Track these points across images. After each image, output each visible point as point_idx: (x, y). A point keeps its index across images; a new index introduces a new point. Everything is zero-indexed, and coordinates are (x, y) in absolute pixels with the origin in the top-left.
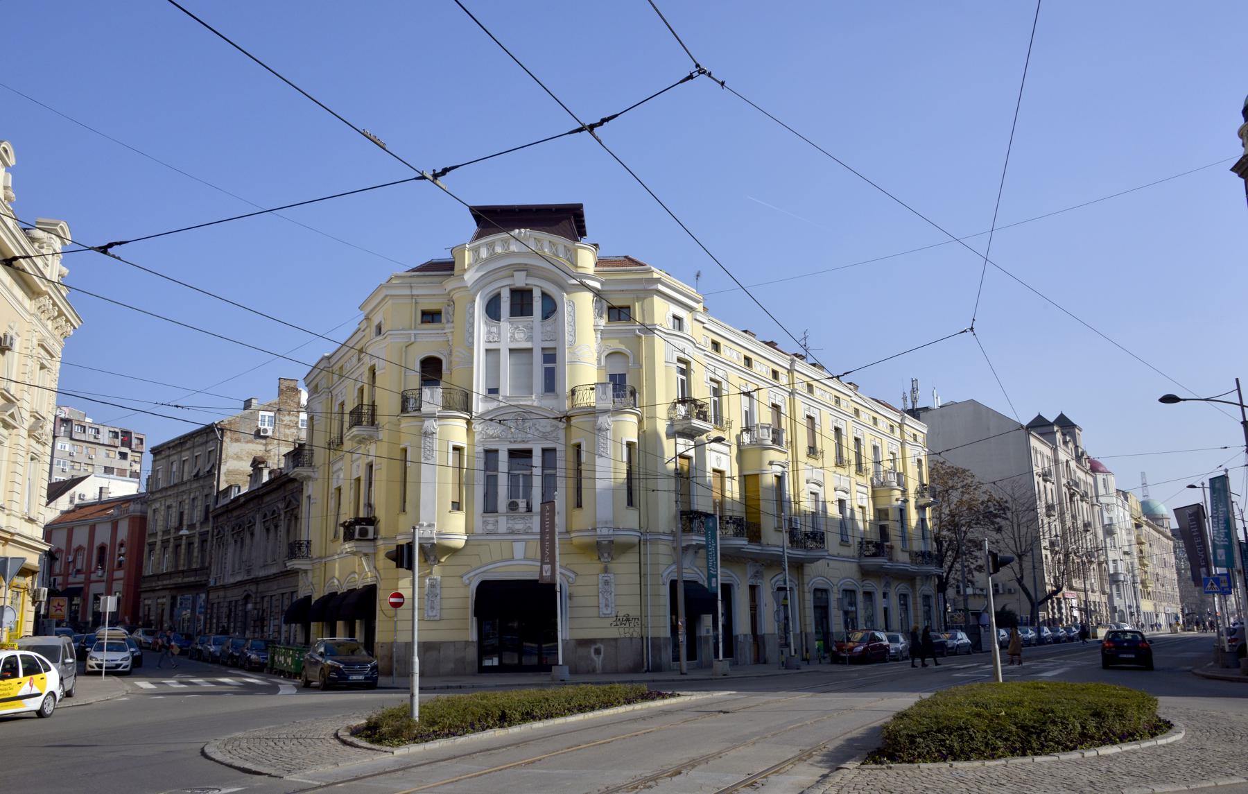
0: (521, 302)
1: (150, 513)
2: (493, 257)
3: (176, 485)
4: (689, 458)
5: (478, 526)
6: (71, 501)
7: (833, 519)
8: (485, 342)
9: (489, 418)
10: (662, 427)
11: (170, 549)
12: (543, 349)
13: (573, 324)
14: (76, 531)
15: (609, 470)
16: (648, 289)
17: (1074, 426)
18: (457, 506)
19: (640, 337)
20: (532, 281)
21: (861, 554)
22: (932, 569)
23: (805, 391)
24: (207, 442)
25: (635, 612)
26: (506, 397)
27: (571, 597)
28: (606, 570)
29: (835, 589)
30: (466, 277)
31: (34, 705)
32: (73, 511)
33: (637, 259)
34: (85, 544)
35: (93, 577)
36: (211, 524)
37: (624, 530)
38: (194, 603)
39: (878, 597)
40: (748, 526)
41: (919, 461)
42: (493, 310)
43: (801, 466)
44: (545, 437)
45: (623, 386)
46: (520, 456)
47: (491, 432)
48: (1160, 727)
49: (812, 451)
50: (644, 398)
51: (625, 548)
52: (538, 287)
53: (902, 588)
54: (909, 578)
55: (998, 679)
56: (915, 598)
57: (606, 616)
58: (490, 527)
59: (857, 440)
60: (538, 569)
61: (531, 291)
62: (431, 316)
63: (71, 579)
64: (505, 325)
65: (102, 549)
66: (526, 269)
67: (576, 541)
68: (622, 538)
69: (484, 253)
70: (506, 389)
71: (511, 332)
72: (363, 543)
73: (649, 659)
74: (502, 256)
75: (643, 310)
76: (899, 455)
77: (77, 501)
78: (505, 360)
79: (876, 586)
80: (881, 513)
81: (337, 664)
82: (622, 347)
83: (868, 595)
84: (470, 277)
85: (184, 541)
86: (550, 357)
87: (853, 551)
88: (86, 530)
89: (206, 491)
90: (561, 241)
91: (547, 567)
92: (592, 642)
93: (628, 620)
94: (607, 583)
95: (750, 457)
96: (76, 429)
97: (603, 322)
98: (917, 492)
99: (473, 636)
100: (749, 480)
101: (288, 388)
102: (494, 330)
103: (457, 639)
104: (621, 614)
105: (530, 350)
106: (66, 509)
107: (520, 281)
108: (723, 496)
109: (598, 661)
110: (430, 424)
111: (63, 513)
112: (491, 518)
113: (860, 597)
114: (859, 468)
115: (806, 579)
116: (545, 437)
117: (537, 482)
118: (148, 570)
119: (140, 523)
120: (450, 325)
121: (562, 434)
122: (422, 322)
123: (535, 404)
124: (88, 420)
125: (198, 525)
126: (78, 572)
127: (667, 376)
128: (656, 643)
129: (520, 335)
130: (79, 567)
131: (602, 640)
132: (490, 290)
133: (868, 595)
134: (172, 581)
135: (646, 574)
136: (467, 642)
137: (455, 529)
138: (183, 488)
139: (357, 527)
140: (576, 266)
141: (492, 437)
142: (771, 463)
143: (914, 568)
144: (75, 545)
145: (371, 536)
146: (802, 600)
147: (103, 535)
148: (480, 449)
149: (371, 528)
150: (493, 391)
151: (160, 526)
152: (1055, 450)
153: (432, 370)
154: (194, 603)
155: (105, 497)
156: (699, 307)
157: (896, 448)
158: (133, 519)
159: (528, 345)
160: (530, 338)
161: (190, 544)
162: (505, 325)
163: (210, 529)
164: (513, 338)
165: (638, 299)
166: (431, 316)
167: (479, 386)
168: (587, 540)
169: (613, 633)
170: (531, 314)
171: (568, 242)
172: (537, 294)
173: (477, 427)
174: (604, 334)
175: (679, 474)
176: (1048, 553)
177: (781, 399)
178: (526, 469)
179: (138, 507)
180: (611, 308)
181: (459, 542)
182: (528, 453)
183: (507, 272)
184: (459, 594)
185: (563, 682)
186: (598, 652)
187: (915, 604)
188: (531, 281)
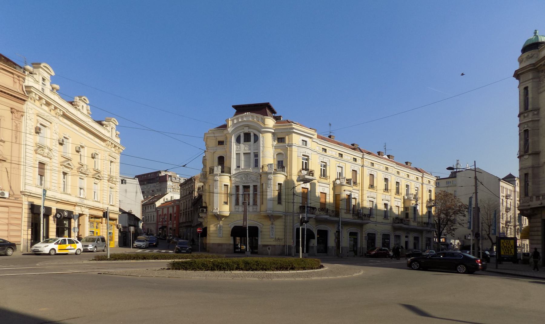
0: (247, 138)
2: (238, 122)
4: (307, 189)
5: (233, 209)
7: (380, 210)
8: (236, 151)
9: (237, 175)
10: (295, 178)
13: (263, 144)
15: (272, 192)
16: (290, 132)
18: (226, 203)
23: (370, 165)
28: (272, 224)
29: (379, 234)
30: (229, 130)
31: (74, 251)
34: (166, 213)
42: (238, 140)
44: (254, 181)
45: (281, 165)
46: (246, 188)
47: (237, 180)
48: (322, 267)
49: (372, 186)
50: (287, 169)
51: (278, 217)
52: (252, 132)
53: (416, 235)
56: (422, 238)
61: (250, 134)
62: (221, 143)
64: (242, 145)
66: (248, 126)
70: (242, 166)
71: (244, 148)
73: (287, 251)
78: (242, 157)
80: (406, 208)
82: (282, 152)
84: (230, 130)
86: (256, 155)
88: (161, 210)
90: (260, 116)
94: (272, 228)
95: (337, 189)
96: (173, 179)
97: (275, 143)
100: (336, 197)
104: (277, 237)
107: (246, 130)
109: (269, 251)
110: (218, 178)
112: (237, 207)
116: (254, 181)
117: (251, 196)
118: (181, 221)
121: (259, 181)
124: (178, 176)
127: (298, 160)
131: (271, 245)
132: (237, 133)
137: (226, 210)
142: (344, 191)
143: (421, 228)
145: (205, 212)
146: (362, 236)
147: (171, 211)
148: (234, 185)
149: (205, 209)
150: (239, 167)
152: (515, 187)
153: (221, 160)
155: (173, 199)
156: (315, 137)
157: (419, 186)
158: (177, 206)
159: (249, 152)
160: (250, 149)
165: (287, 135)
166: (221, 143)
169: (274, 243)
170: (250, 141)
171: (262, 116)
172: (252, 134)
173: (233, 179)
174: (276, 147)
175: (303, 193)
177: (358, 168)
178: (247, 192)
181: (227, 214)
184: (228, 230)
185: (248, 256)
186: (269, 249)
187: (422, 240)
188: (250, 130)
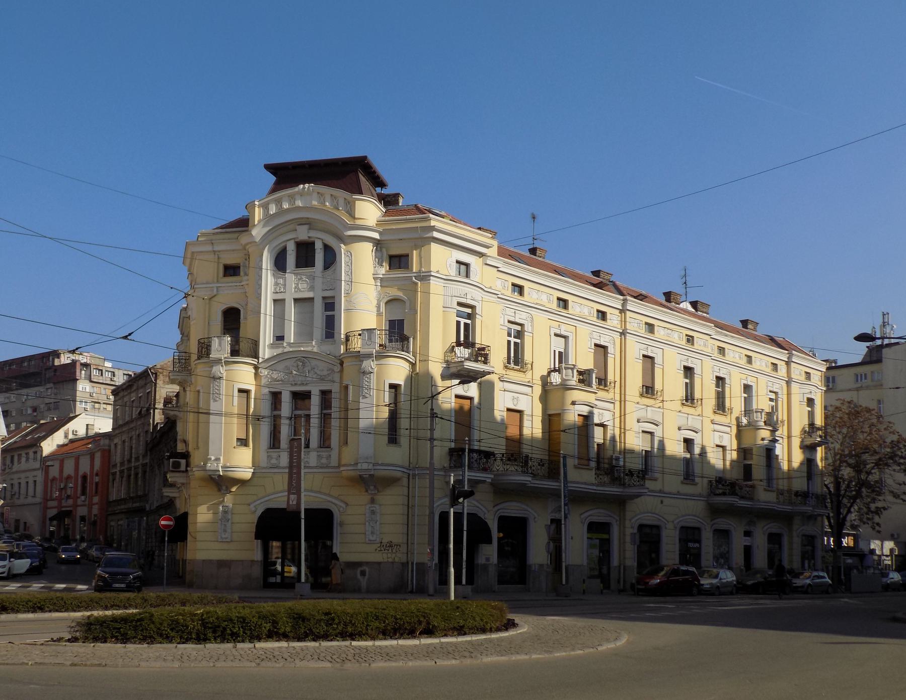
0: (305, 254)
1: (113, 447)
2: (281, 212)
3: (127, 423)
6: (66, 436)
7: (673, 458)
10: (436, 369)
11: (124, 479)
12: (324, 298)
13: (350, 273)
14: (66, 462)
15: (374, 410)
16: (424, 238)
18: (243, 442)
19: (417, 284)
20: (313, 234)
24: (146, 384)
25: (398, 539)
26: (289, 344)
27: (341, 524)
28: (373, 501)
29: (670, 526)
32: (66, 445)
35: (79, 502)
36: (149, 457)
37: (382, 465)
38: (140, 524)
40: (552, 465)
41: (810, 402)
42: (280, 264)
43: (630, 407)
44: (322, 379)
45: (399, 333)
46: (301, 397)
49: (649, 390)
51: (390, 482)
52: (320, 240)
53: (774, 527)
55: (447, 594)
57: (371, 542)
58: (274, 461)
60: (286, 499)
61: (313, 244)
62: (231, 270)
63: (64, 504)
64: (291, 278)
65: (84, 477)
66: (309, 223)
67: (344, 473)
68: (382, 472)
69: (273, 209)
70: (291, 336)
71: (295, 284)
72: (177, 474)
74: (288, 211)
75: (420, 257)
76: (783, 397)
77: (71, 436)
78: (291, 311)
80: (744, 452)
81: (104, 574)
82: (400, 294)
83: (723, 534)
84: (257, 232)
85: (140, 470)
86: (330, 305)
88: (57, 464)
89: (146, 429)
90: (341, 194)
91: (293, 497)
92: (359, 564)
93: (391, 546)
94: (373, 512)
95: (553, 397)
96: (95, 373)
97: (383, 270)
98: (804, 431)
100: (551, 420)
102: (281, 281)
104: (385, 541)
105: (311, 300)
106: (61, 443)
107: (303, 234)
108: (521, 434)
109: (364, 582)
110: (221, 370)
111: (59, 446)
112: (274, 453)
114: (721, 406)
115: (629, 515)
116: (322, 379)
117: (315, 422)
118: (113, 497)
119: (107, 454)
120: (246, 278)
121: (337, 377)
122: (225, 275)
123: (315, 350)
124: (108, 364)
125: (141, 457)
126: (68, 497)
128: (422, 568)
129: (303, 286)
130: (69, 493)
131: (367, 563)
132: (278, 243)
133: (723, 534)
134: (126, 506)
135: (413, 506)
136: (252, 561)
137: (242, 462)
138: (132, 425)
140: (354, 218)
141: (276, 380)
142: (573, 403)
143: (788, 508)
144: (65, 475)
145: (183, 468)
147: (85, 467)
149: (183, 462)
150: (280, 338)
151: (118, 459)
153: (232, 320)
154: (140, 524)
155: (91, 433)
156: (493, 252)
157: (780, 386)
160: (312, 288)
161: (136, 474)
162: (291, 278)
163: (148, 461)
165: (416, 247)
166: (231, 270)
167: (266, 336)
168: (352, 473)
172: (319, 246)
173: (264, 372)
174: (384, 282)
175: (459, 411)
178: (303, 411)
179: (107, 442)
180: (391, 257)
183: (292, 227)
184: (246, 519)
185: (302, 597)
186: (363, 573)
188: (313, 234)
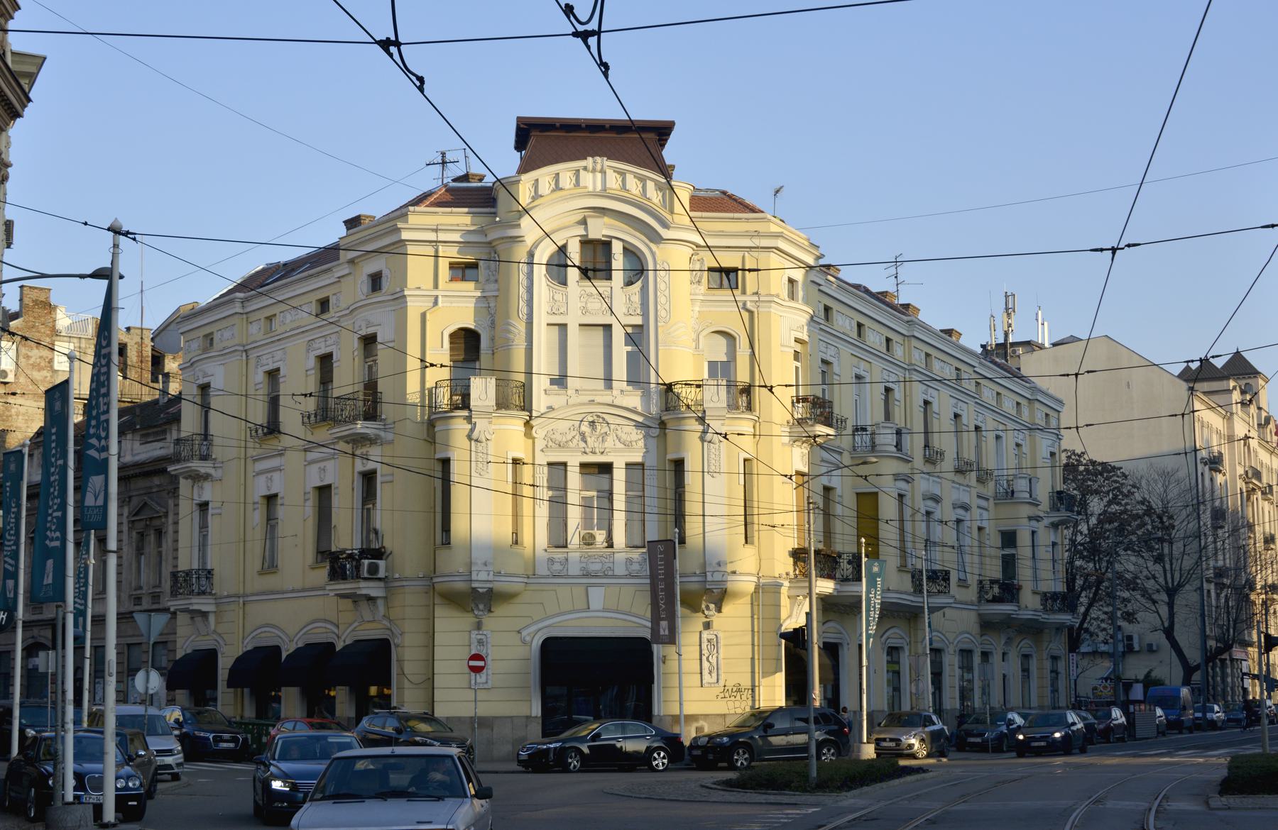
17: (1255, 373)
21: (980, 598)
22: (1065, 618)
29: (951, 649)
33: (749, 200)
39: (996, 658)
53: (1026, 645)
54: (1033, 629)
59: (926, 403)
79: (996, 644)
83: (985, 655)
86: (637, 336)
87: (971, 594)
93: (739, 691)
99: (536, 710)
101: (36, 302)
103: (515, 714)
107: (599, 229)
113: (977, 659)
131: (706, 716)
133: (985, 655)
136: (528, 718)
139: (366, 562)
145: (382, 574)
149: (381, 563)
164: (585, 311)
172: (617, 248)
176: (1212, 587)
182: (606, 468)
